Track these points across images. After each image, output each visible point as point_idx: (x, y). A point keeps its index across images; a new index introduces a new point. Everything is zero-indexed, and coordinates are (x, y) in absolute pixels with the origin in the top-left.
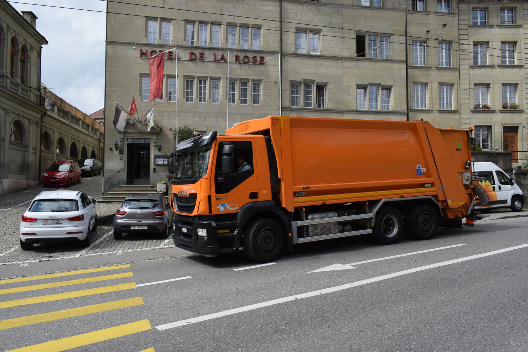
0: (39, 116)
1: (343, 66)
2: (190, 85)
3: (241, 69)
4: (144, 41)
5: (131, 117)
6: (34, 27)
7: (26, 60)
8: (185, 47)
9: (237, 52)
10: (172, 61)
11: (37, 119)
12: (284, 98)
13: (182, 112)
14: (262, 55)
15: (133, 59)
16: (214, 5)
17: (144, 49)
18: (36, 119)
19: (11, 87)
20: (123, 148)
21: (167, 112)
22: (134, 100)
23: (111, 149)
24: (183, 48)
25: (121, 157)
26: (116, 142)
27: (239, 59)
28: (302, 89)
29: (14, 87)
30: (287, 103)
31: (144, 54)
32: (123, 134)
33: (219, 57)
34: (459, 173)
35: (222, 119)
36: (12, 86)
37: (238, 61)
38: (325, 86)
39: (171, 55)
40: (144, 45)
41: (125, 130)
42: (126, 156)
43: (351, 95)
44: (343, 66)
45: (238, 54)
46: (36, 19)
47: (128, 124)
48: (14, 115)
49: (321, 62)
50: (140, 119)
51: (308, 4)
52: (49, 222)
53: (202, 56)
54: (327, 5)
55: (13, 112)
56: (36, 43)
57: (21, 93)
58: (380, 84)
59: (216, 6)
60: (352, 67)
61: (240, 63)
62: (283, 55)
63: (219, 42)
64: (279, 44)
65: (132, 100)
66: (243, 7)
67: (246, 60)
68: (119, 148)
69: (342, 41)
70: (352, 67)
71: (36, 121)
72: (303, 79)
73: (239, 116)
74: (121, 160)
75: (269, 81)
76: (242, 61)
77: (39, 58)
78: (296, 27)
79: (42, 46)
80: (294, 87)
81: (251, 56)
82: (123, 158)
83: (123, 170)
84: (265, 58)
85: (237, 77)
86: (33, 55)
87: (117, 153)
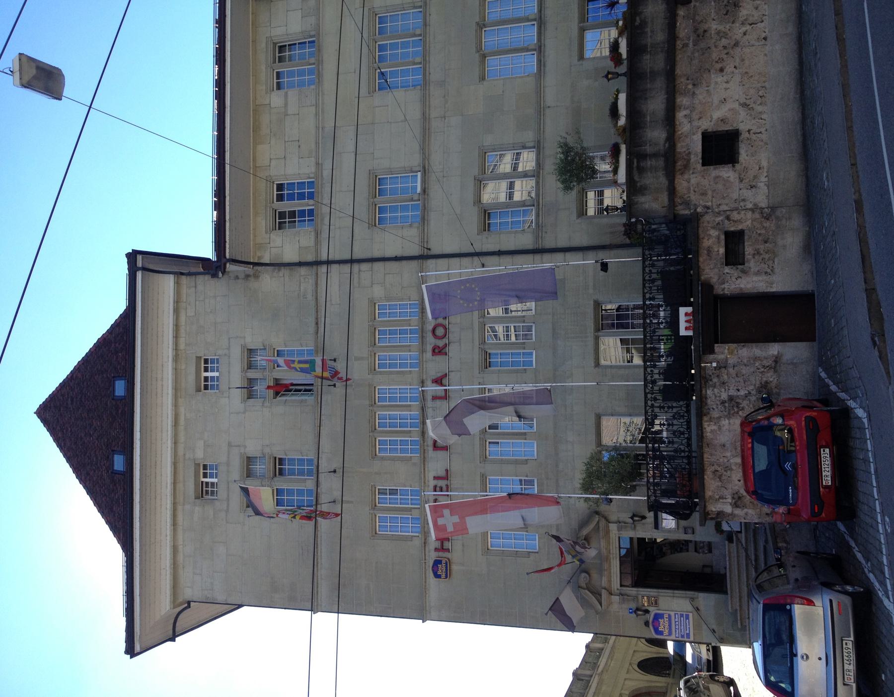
8: (424, 460)
9: (426, 352)
12: (322, 452)
13: (557, 466)
24: (426, 463)
26: (631, 613)
30: (574, 553)
34: (447, 471)
42: (660, 590)
43: (503, 92)
44: (442, 117)
45: (429, 348)
46: (421, 621)
52: (745, 624)
64: (404, 263)
67: (440, 331)
69: (391, 123)
83: (692, 599)
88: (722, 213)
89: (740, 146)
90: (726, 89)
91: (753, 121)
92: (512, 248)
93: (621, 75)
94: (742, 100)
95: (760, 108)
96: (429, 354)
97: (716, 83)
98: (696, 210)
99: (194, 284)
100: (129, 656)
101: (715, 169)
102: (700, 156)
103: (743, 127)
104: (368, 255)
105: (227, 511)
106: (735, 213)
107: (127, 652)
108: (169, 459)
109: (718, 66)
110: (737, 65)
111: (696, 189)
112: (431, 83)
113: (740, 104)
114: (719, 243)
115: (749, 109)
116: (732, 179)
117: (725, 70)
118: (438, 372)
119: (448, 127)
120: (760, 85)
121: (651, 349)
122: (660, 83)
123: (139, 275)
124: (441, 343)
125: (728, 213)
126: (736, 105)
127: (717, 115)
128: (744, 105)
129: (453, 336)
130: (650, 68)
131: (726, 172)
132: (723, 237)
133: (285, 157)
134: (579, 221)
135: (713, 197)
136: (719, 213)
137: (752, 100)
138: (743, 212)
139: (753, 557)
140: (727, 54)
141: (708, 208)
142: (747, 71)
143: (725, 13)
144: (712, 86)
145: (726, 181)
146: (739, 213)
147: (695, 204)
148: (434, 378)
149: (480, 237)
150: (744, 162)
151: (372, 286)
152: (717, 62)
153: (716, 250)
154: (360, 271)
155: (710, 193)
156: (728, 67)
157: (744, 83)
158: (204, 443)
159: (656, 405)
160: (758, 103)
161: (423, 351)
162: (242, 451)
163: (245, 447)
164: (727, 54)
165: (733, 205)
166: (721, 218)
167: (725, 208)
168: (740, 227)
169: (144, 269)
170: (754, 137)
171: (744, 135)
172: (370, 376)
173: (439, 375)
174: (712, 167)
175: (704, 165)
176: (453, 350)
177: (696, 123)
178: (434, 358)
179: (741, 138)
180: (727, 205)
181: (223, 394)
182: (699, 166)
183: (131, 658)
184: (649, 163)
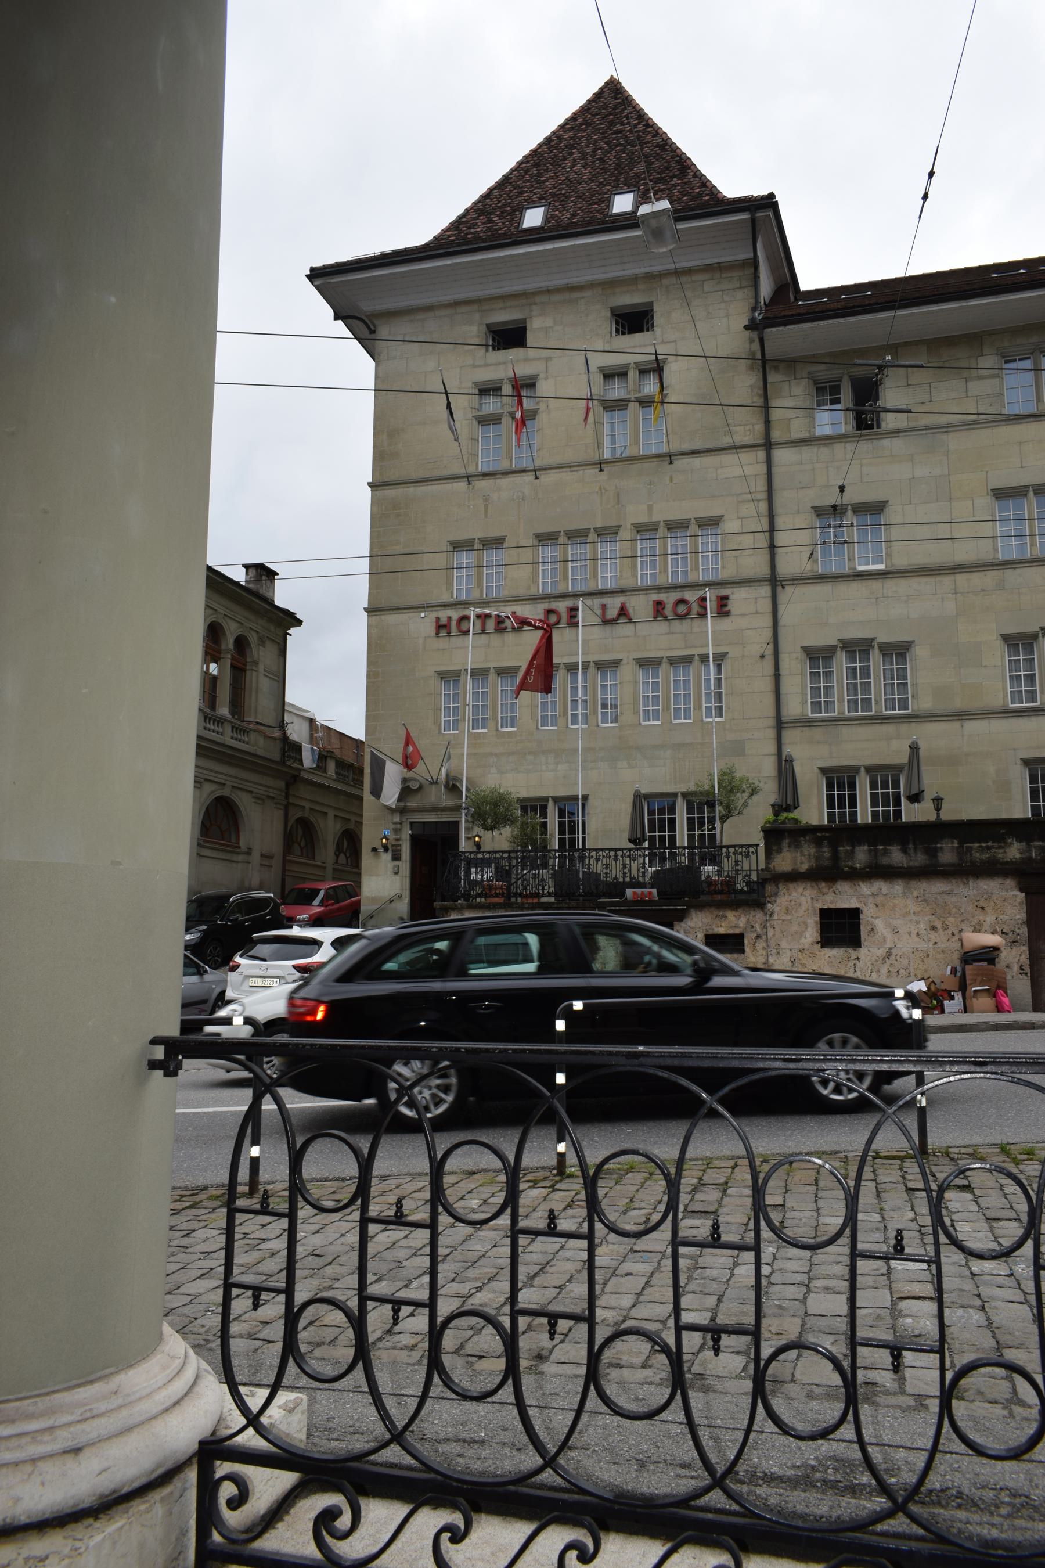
0: (282, 784)
1: (955, 589)
2: (1021, 658)
3: (670, 633)
4: (445, 598)
5: (410, 774)
6: (268, 595)
7: (248, 668)
10: (506, 634)
11: (275, 792)
13: (530, 753)
14: (724, 592)
15: (421, 641)
16: (600, 488)
17: (444, 615)
18: (271, 790)
19: (205, 728)
20: (400, 845)
21: (496, 755)
22: (408, 735)
23: (374, 850)
25: (395, 866)
27: (663, 609)
28: (841, 662)
29: (212, 727)
31: (444, 626)
32: (398, 814)
33: (612, 613)
35: (625, 764)
36: (208, 725)
37: (662, 616)
38: (910, 646)
39: (726, 605)
40: (445, 606)
41: (402, 804)
43: (985, 666)
44: (955, 589)
45: (662, 597)
47: (406, 791)
48: (213, 787)
49: (892, 586)
50: (435, 778)
51: (846, 442)
53: (573, 613)
54: (901, 434)
55: (206, 780)
56: (272, 628)
57: (232, 738)
58: (873, 639)
59: (606, 491)
60: (983, 590)
61: (666, 618)
62: (775, 582)
63: (607, 577)
65: (404, 736)
66: (671, 480)
67: (682, 609)
68: (393, 846)
70: (983, 590)
71: (272, 795)
72: (840, 640)
73: (669, 752)
74: (396, 873)
75: (743, 656)
76: (672, 614)
77: (282, 659)
78: (813, 508)
79: (288, 632)
80: (892, 658)
81: (691, 596)
82: (400, 869)
84: (731, 597)
85: (659, 654)
86: (264, 655)
87: (386, 857)
88: (765, 930)
89: (842, 949)
90: (910, 934)
91: (869, 964)
92: (784, 689)
93: (938, 814)
94: (894, 951)
95: (884, 970)
96: (655, 597)
97: (918, 923)
98: (769, 902)
99: (743, 285)
100: (309, 273)
101: (816, 922)
102: (832, 906)
103: (863, 952)
104: (778, 509)
105: (474, 366)
106: (765, 945)
107: (312, 269)
108: (531, 286)
109: (938, 925)
110: (939, 945)
111: (793, 903)
112: (1001, 571)
113: (890, 949)
114: (731, 927)
115: (884, 959)
116: (803, 940)
117: (933, 932)
118: (634, 610)
119: (942, 599)
120: (912, 970)
121: (616, 856)
122: (919, 859)
123: (745, 216)
124: (668, 611)
125: (764, 937)
126: (889, 944)
127: (880, 924)
128: (889, 954)
129: (677, 626)
130: (941, 848)
131: (812, 933)
132: (737, 931)
133: (909, 385)
134: (816, 770)
135: (783, 921)
136: (765, 927)
137: (894, 962)
138: (764, 953)
139: (982, 1075)
140: (953, 934)
141: (771, 915)
142: (930, 956)
143: (1004, 931)
144: (915, 918)
145: (800, 934)
146: (764, 948)
147: (775, 901)
148: (627, 605)
149: (799, 649)
150: (822, 953)
151: (738, 518)
152: (943, 922)
153: (723, 924)
154: (759, 501)
155: (789, 917)
156: (936, 935)
157: (916, 953)
158: (550, 327)
159: (592, 860)
160: (891, 969)
161: (659, 589)
162: (542, 376)
163: (546, 379)
164: (953, 934)
165: (773, 943)
166: (758, 929)
167: (771, 932)
168: (747, 949)
169: (753, 221)
170: (851, 964)
171: (853, 953)
172: (629, 526)
173: (631, 611)
174: (818, 919)
175: (822, 911)
176: (661, 627)
177: (871, 900)
178: (651, 603)
179: (850, 950)
180: (774, 935)
181: (608, 342)
182: (819, 905)
183: (307, 276)
184: (826, 849)
